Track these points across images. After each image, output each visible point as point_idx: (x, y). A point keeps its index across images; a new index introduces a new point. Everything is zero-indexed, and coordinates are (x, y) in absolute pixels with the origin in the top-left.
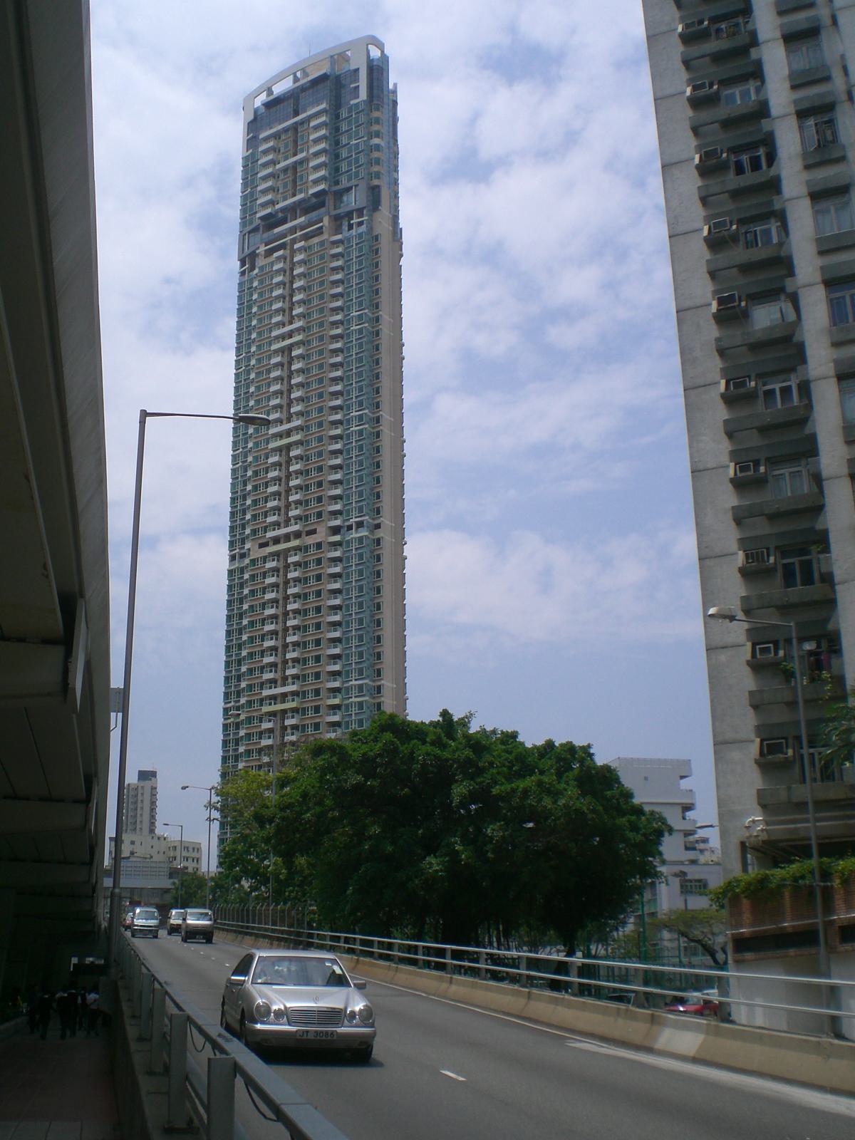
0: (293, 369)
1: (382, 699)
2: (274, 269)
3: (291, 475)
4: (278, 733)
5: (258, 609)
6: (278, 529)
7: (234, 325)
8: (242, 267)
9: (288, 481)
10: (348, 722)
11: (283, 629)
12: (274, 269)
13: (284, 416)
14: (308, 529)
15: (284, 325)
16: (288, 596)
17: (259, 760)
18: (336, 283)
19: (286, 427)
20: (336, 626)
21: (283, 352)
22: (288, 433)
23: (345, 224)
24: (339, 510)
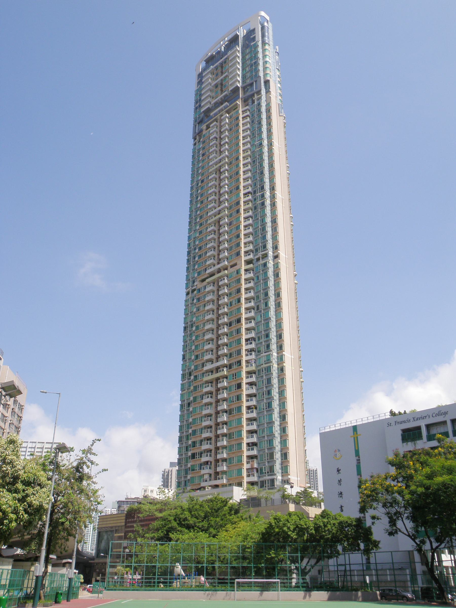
0: (219, 333)
1: (289, 477)
2: (207, 247)
3: (220, 347)
4: (213, 441)
5: (198, 456)
6: (211, 374)
7: (179, 397)
8: (194, 141)
9: (217, 395)
10: (263, 455)
11: (215, 413)
12: (207, 247)
13: (214, 357)
14: (231, 264)
15: (215, 208)
16: (219, 423)
17: (200, 484)
18: (247, 218)
19: (217, 267)
20: (251, 374)
21: (214, 283)
22: (217, 369)
23: (250, 101)
24: (254, 370)
